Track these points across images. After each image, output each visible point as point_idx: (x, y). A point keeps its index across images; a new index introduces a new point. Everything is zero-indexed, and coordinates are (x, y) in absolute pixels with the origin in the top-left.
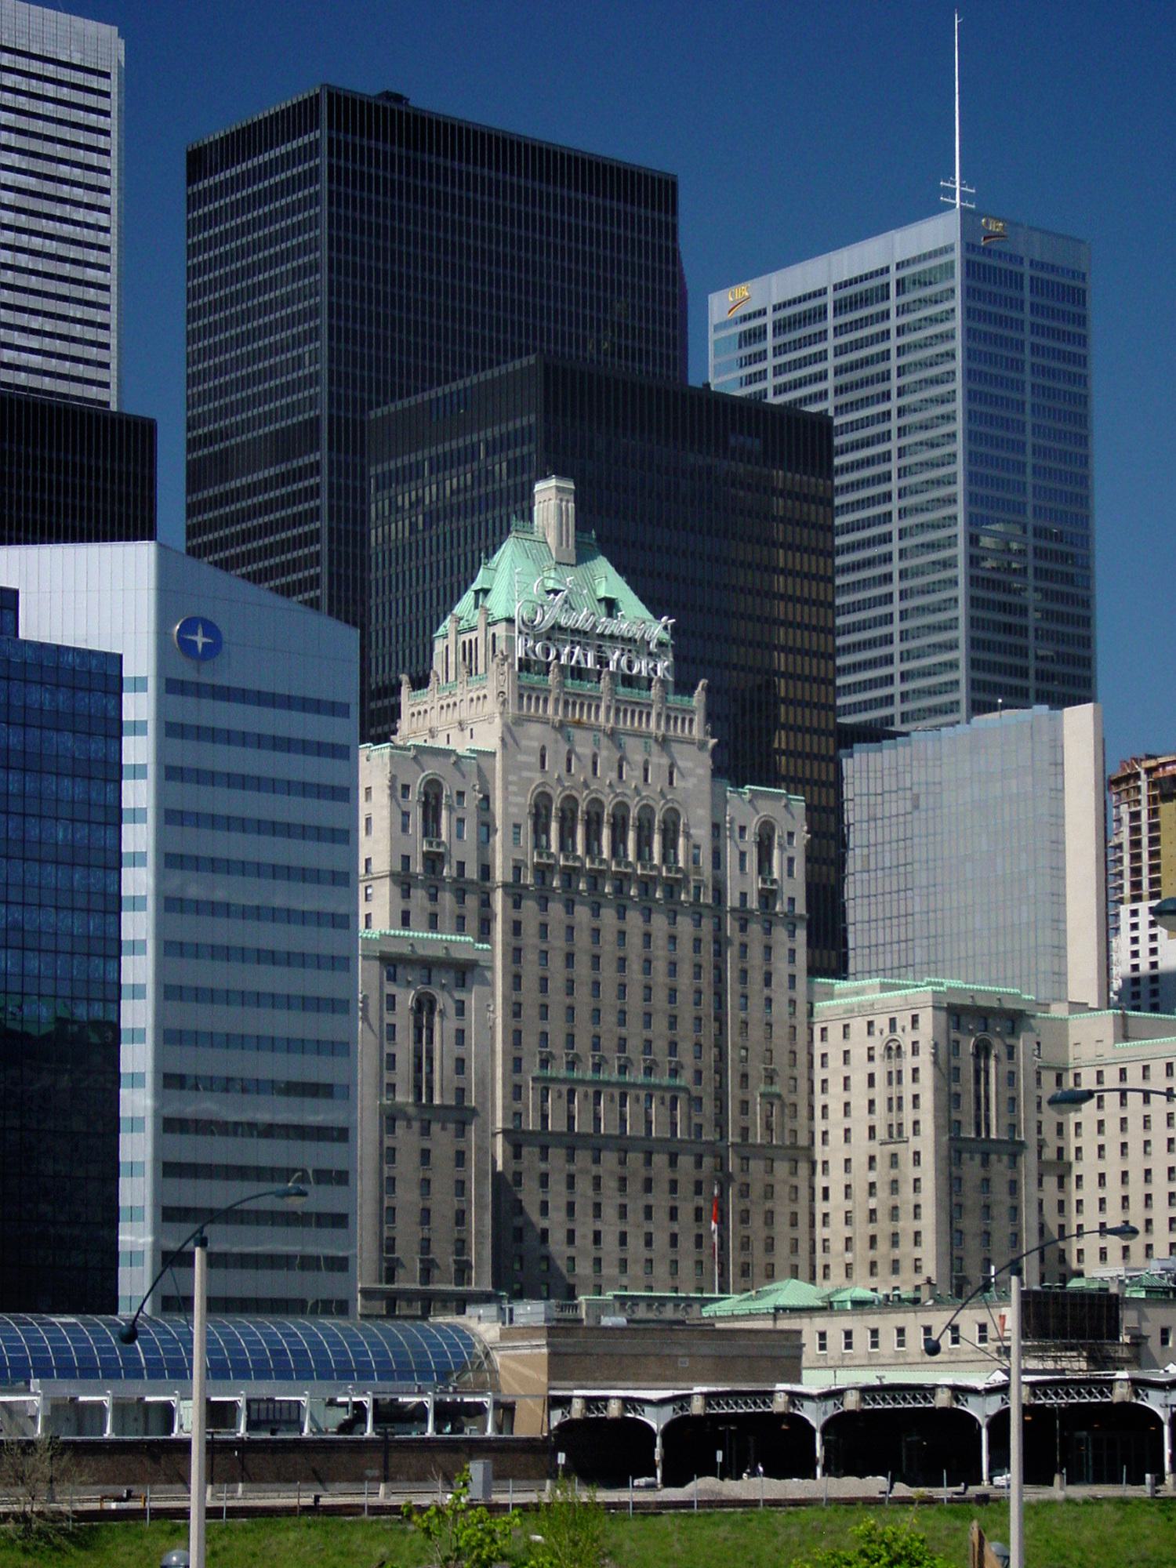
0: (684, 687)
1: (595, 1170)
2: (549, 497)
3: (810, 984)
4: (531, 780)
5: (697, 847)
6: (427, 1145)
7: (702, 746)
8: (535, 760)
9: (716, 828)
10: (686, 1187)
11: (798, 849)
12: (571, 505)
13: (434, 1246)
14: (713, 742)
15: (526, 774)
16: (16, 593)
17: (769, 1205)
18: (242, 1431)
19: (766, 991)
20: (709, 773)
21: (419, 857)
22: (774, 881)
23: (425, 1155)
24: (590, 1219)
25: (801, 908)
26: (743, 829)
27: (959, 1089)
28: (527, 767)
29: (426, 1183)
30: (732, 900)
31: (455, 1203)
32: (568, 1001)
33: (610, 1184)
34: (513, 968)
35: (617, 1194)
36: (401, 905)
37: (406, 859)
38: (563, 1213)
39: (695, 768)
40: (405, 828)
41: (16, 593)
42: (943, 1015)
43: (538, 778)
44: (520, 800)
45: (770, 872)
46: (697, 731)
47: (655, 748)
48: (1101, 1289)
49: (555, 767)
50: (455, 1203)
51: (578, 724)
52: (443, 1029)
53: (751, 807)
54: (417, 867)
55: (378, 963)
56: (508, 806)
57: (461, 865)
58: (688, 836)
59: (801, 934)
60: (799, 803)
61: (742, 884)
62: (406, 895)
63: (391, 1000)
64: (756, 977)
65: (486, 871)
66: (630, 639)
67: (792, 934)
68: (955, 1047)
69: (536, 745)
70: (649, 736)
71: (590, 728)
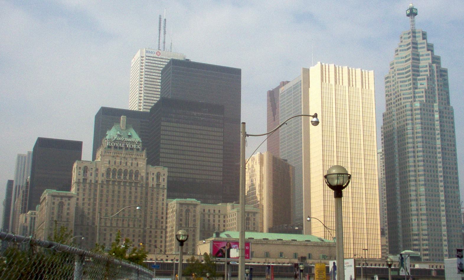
0: (143, 150)
3: (167, 200)
4: (106, 166)
5: (142, 177)
7: (144, 159)
8: (108, 162)
9: (147, 174)
11: (166, 177)
12: (125, 120)
14: (147, 159)
16: (237, 72)
17: (156, 239)
20: (146, 164)
21: (82, 179)
22: (160, 182)
25: (166, 187)
26: (153, 174)
27: (182, 218)
30: (150, 185)
36: (77, 187)
37: (79, 180)
39: (142, 163)
41: (237, 72)
42: (178, 205)
43: (108, 165)
44: (104, 169)
45: (159, 180)
46: (144, 157)
47: (134, 160)
48: (412, 224)
49: (112, 163)
51: (117, 156)
53: (154, 170)
54: (81, 181)
56: (103, 170)
57: (91, 181)
58: (140, 174)
59: (166, 191)
60: (166, 169)
61: (152, 182)
62: (78, 186)
64: (155, 199)
65: (97, 182)
66: (132, 142)
67: (163, 192)
68: (181, 210)
69: (108, 160)
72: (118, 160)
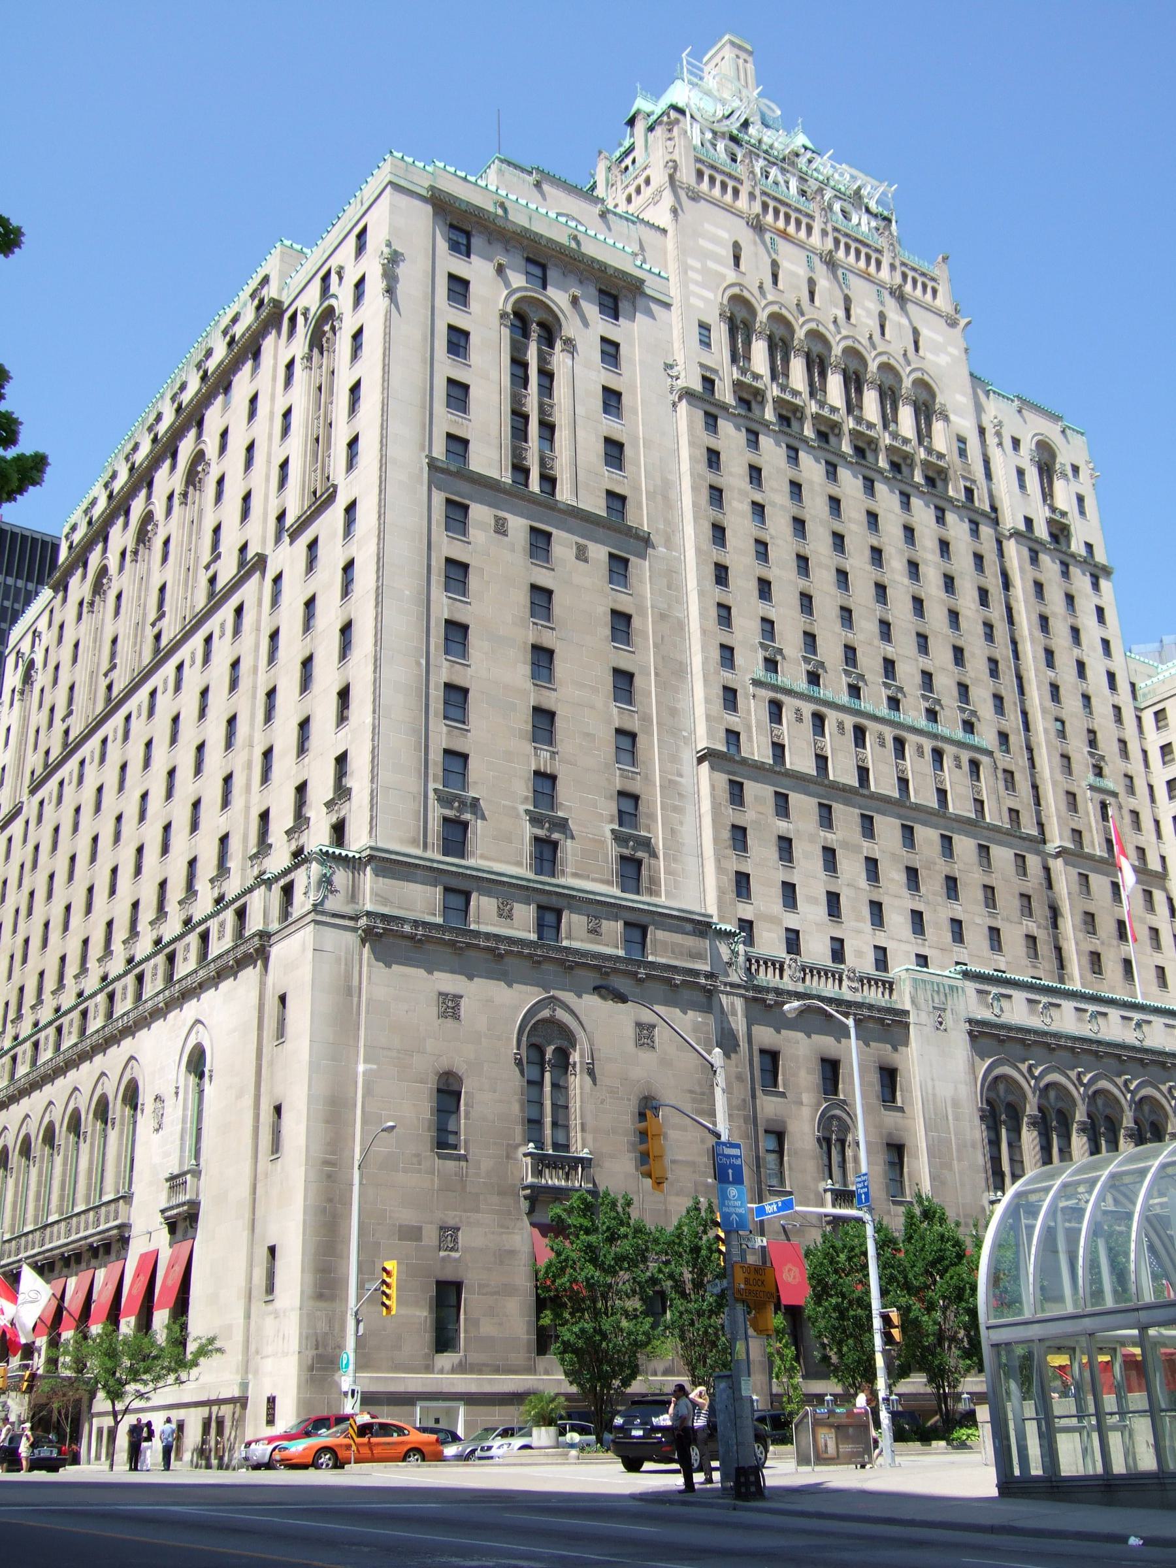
1: (868, 848)
2: (574, 1389)
6: (544, 578)
10: (1008, 901)
13: (565, 792)
15: (711, 265)
18: (1024, 1221)
19: (1076, 652)
23: (541, 598)
24: (867, 926)
28: (717, 259)
29: (542, 659)
31: (616, 715)
32: (802, 584)
33: (893, 876)
34: (712, 514)
35: (905, 892)
38: (822, 909)
40: (706, 343)
43: (731, 276)
44: (710, 296)
49: (755, 268)
50: (616, 715)
52: (578, 374)
55: (429, 209)
63: (459, 288)
69: (727, 237)
70: (881, 285)
71: (801, 245)
72: (794, 266)
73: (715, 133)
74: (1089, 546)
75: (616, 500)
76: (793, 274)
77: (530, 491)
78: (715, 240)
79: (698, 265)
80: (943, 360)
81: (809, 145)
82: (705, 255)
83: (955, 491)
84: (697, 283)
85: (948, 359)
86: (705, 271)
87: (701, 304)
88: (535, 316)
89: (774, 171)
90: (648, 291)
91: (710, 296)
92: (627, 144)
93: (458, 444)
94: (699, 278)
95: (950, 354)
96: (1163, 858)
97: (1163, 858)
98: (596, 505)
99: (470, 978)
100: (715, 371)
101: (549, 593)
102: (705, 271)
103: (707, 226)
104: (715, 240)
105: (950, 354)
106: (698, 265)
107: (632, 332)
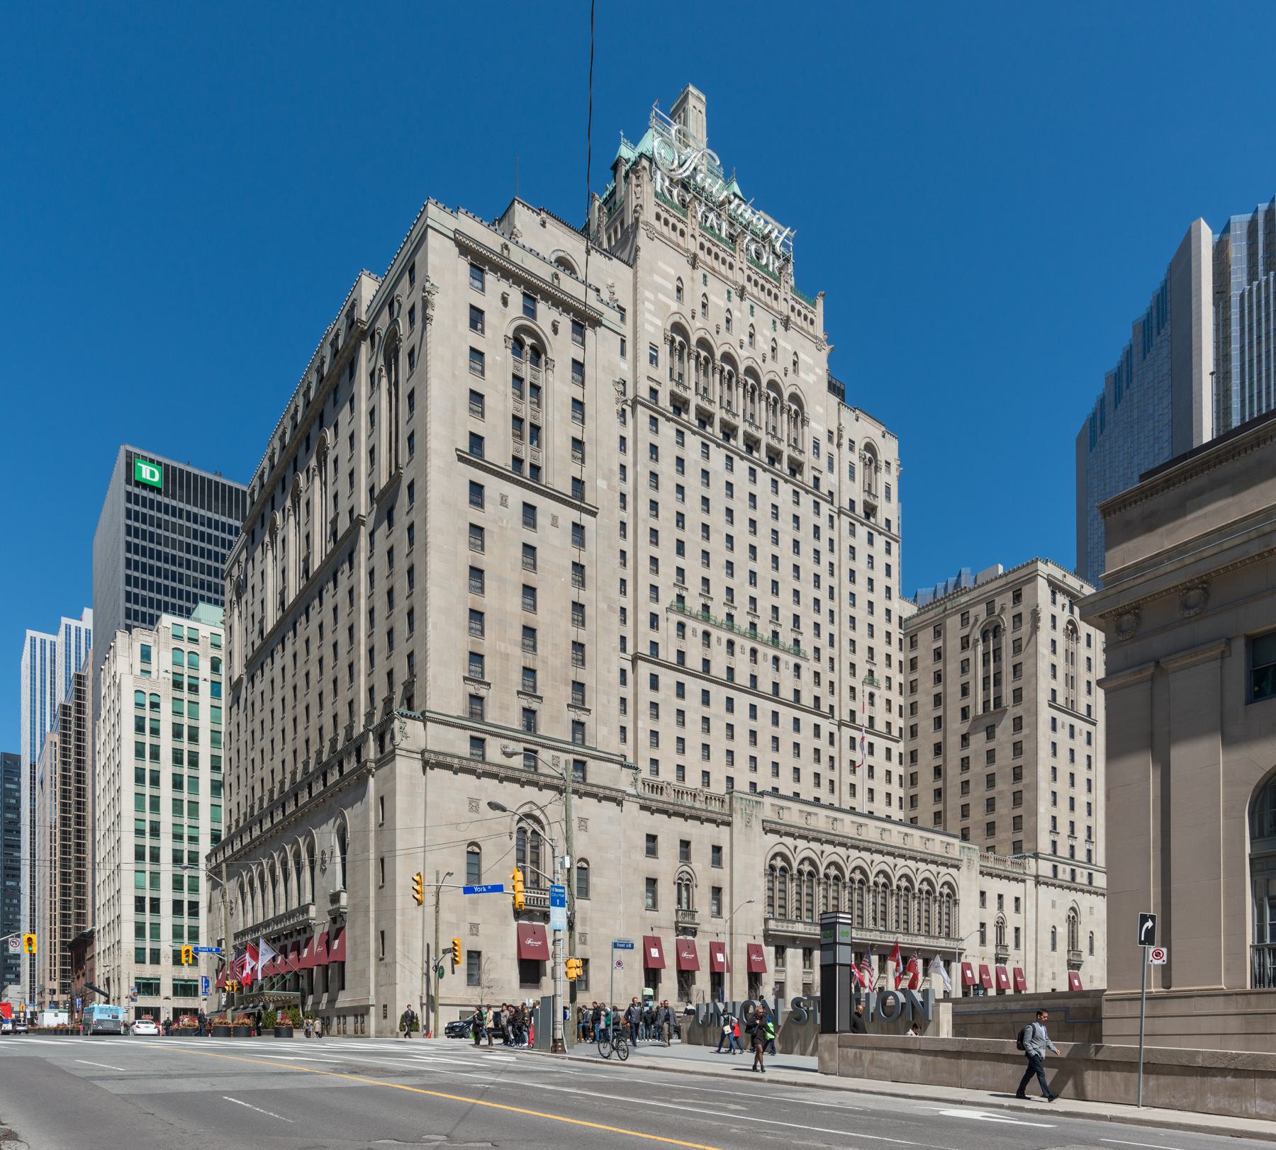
15: (661, 296)
43: (674, 306)
44: (659, 323)
52: (558, 386)
73: (671, 180)
74: (888, 522)
75: (578, 483)
76: (717, 306)
77: (526, 473)
78: (665, 276)
79: (652, 297)
80: (811, 378)
81: (739, 193)
82: (658, 289)
83: (807, 477)
84: (650, 311)
85: (815, 378)
86: (656, 302)
87: (651, 329)
88: (529, 341)
89: (711, 216)
90: (604, 322)
91: (659, 323)
92: (611, 188)
93: (476, 441)
94: (652, 307)
95: (816, 374)
96: (1089, 707)
97: (1089, 707)
98: (566, 488)
99: (1105, 650)
100: (659, 383)
101: (534, 508)
102: (656, 302)
103: (660, 264)
104: (665, 276)
105: (816, 374)
106: (652, 297)
107: (600, 345)
